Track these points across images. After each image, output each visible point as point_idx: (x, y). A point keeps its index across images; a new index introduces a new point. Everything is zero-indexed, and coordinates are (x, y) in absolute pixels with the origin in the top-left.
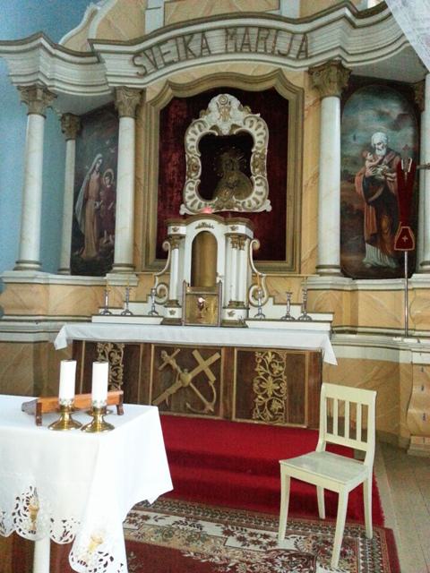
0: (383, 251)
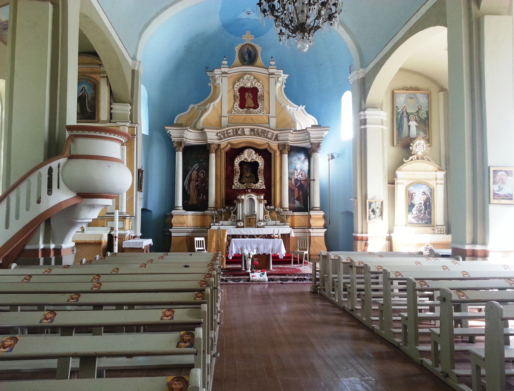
0: (300, 202)
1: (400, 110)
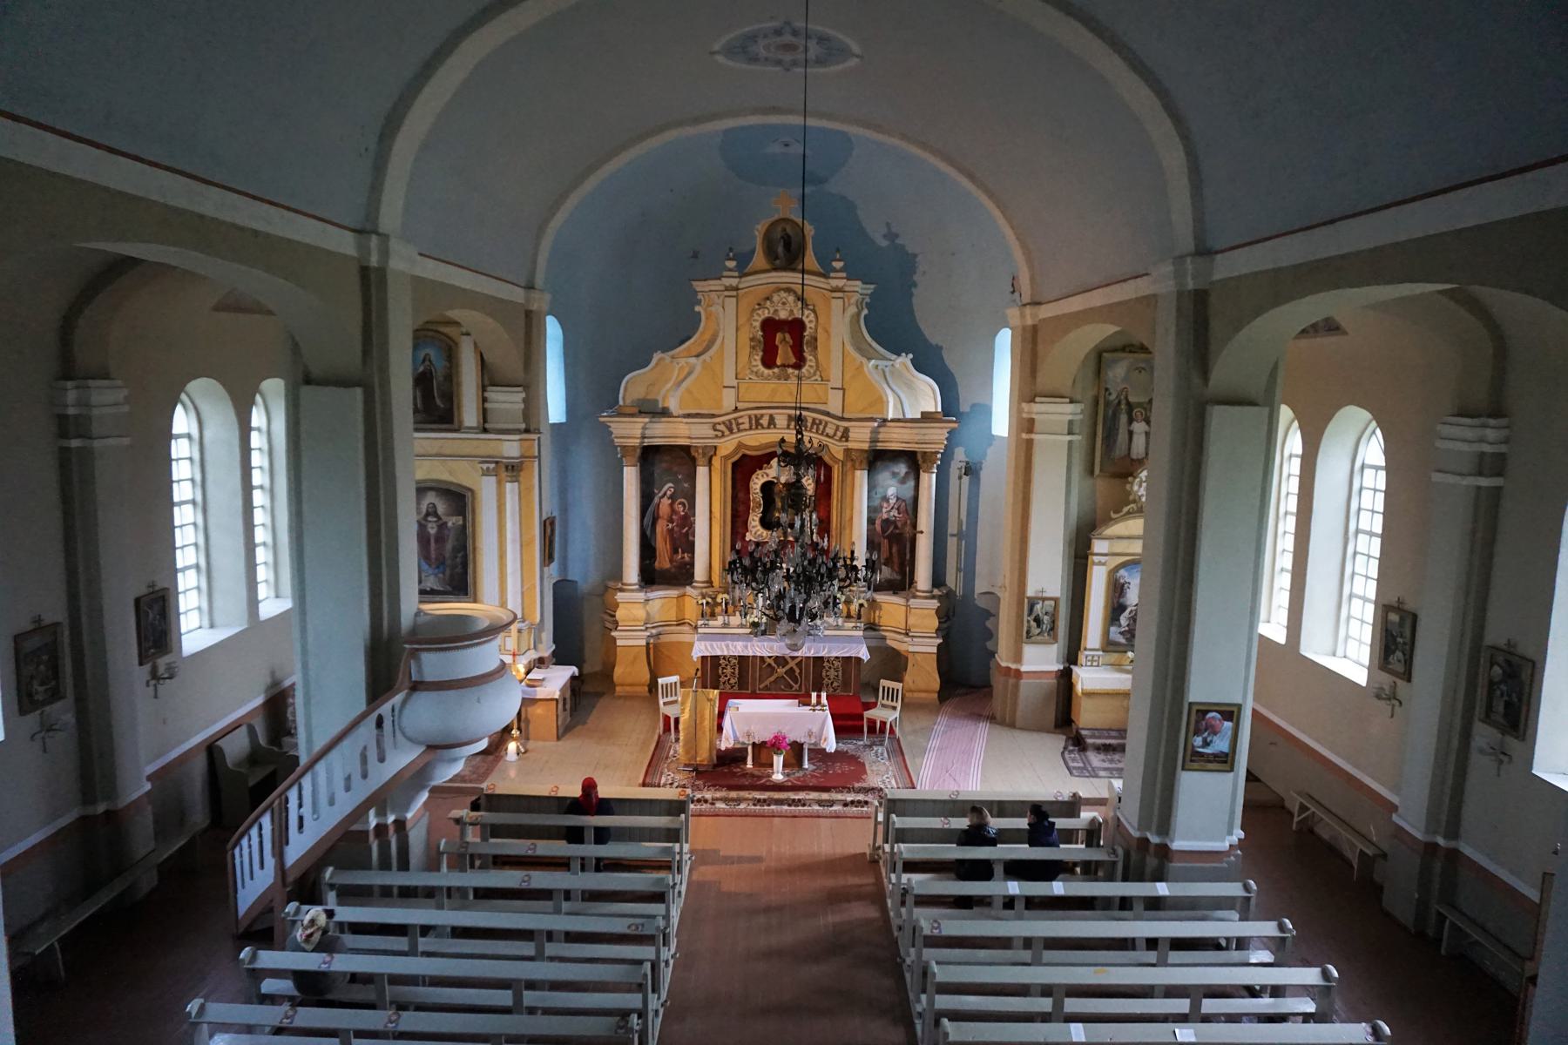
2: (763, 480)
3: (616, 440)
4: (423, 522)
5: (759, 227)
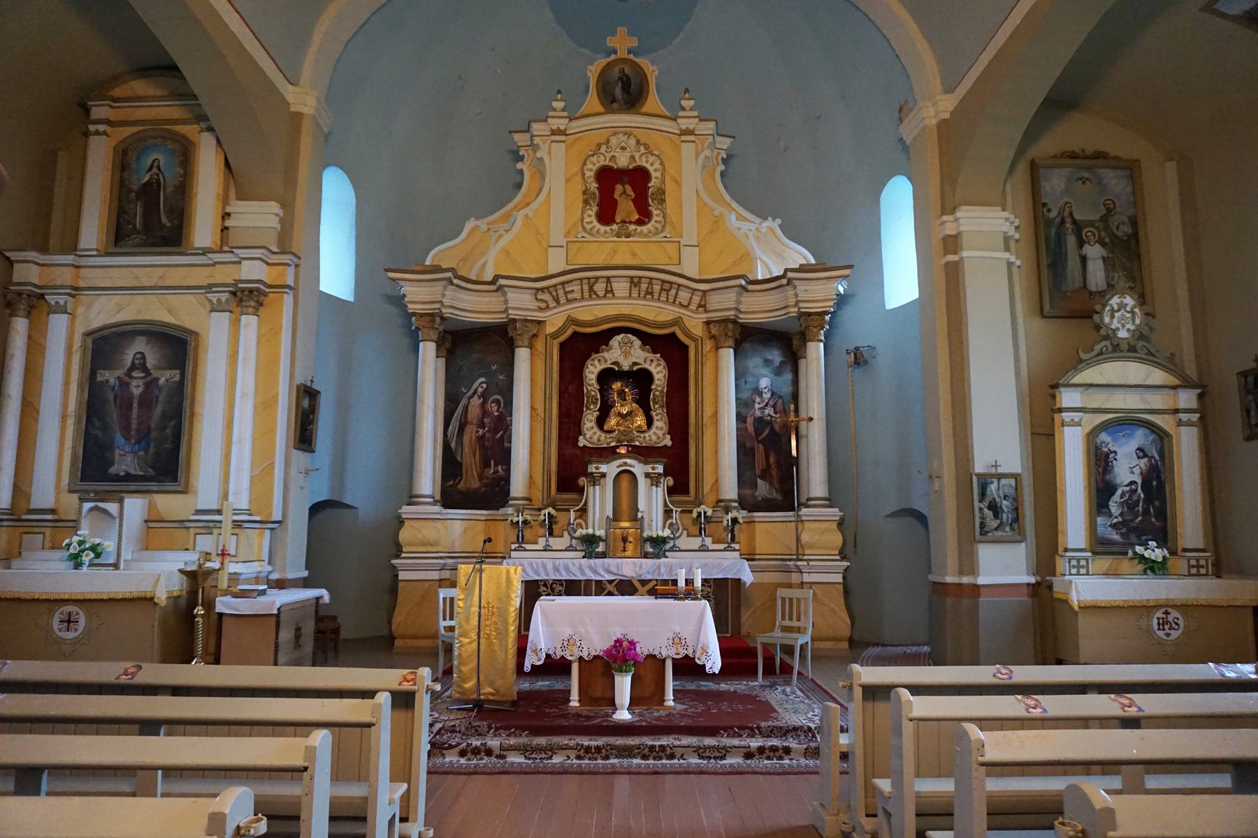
0: (771, 484)
1: (1053, 214)
2: (599, 367)
3: (410, 306)
4: (126, 379)
5: (592, 68)
